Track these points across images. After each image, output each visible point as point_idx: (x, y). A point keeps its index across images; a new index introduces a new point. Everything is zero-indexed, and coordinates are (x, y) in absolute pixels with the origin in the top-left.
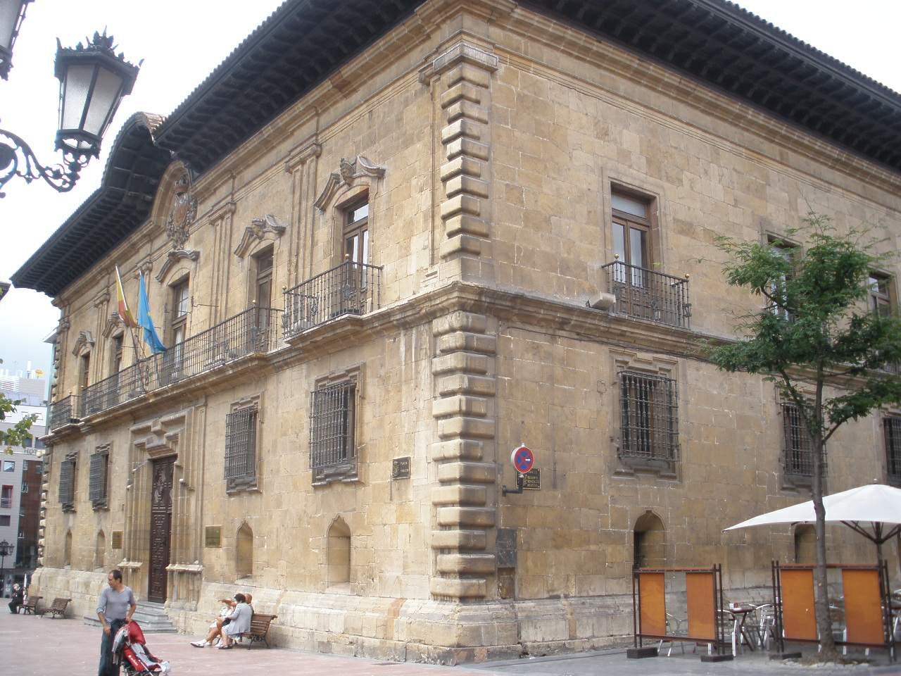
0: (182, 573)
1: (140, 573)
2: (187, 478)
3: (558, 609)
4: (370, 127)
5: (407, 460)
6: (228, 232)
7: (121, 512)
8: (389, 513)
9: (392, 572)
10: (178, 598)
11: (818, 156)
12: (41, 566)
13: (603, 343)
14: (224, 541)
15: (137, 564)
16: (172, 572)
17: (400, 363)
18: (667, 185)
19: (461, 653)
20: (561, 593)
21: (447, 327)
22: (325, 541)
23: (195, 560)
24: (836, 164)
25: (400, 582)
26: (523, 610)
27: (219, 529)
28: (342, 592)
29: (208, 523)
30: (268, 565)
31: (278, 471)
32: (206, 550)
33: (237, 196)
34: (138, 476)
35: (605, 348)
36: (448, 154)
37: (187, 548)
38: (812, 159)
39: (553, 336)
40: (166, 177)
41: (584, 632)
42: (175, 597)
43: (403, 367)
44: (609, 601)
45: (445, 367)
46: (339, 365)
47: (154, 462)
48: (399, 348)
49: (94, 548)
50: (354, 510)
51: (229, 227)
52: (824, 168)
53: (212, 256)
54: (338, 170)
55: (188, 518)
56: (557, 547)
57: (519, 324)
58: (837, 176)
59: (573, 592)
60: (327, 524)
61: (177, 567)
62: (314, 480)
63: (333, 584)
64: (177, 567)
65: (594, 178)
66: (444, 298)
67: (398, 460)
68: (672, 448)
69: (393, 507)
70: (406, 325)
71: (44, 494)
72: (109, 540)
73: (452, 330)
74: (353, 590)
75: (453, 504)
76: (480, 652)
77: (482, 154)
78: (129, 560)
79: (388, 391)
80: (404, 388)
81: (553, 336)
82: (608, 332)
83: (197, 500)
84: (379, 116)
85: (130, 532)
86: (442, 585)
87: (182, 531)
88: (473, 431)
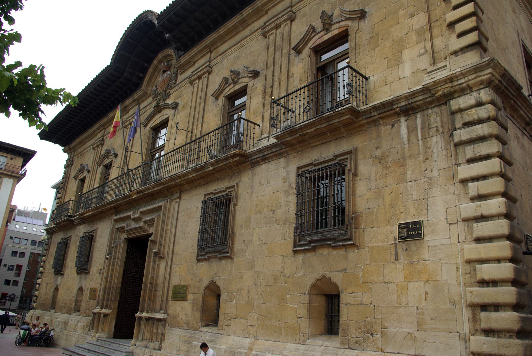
0: (148, 319)
1: (109, 319)
5: (419, 223)
8: (397, 272)
9: (400, 328)
10: (143, 339)
12: (33, 308)
14: (190, 296)
16: (140, 318)
17: (402, 143)
22: (307, 297)
23: (161, 309)
25: (414, 339)
29: (175, 281)
31: (252, 241)
32: (171, 302)
33: (212, 63)
34: (116, 249)
37: (154, 301)
42: (140, 337)
43: (406, 146)
45: (473, 135)
48: (399, 131)
49: (75, 299)
50: (345, 270)
53: (189, 103)
55: (157, 278)
60: (309, 281)
61: (145, 315)
63: (313, 336)
69: (400, 266)
70: (409, 111)
72: (86, 294)
73: (479, 104)
83: (166, 265)
87: (151, 288)
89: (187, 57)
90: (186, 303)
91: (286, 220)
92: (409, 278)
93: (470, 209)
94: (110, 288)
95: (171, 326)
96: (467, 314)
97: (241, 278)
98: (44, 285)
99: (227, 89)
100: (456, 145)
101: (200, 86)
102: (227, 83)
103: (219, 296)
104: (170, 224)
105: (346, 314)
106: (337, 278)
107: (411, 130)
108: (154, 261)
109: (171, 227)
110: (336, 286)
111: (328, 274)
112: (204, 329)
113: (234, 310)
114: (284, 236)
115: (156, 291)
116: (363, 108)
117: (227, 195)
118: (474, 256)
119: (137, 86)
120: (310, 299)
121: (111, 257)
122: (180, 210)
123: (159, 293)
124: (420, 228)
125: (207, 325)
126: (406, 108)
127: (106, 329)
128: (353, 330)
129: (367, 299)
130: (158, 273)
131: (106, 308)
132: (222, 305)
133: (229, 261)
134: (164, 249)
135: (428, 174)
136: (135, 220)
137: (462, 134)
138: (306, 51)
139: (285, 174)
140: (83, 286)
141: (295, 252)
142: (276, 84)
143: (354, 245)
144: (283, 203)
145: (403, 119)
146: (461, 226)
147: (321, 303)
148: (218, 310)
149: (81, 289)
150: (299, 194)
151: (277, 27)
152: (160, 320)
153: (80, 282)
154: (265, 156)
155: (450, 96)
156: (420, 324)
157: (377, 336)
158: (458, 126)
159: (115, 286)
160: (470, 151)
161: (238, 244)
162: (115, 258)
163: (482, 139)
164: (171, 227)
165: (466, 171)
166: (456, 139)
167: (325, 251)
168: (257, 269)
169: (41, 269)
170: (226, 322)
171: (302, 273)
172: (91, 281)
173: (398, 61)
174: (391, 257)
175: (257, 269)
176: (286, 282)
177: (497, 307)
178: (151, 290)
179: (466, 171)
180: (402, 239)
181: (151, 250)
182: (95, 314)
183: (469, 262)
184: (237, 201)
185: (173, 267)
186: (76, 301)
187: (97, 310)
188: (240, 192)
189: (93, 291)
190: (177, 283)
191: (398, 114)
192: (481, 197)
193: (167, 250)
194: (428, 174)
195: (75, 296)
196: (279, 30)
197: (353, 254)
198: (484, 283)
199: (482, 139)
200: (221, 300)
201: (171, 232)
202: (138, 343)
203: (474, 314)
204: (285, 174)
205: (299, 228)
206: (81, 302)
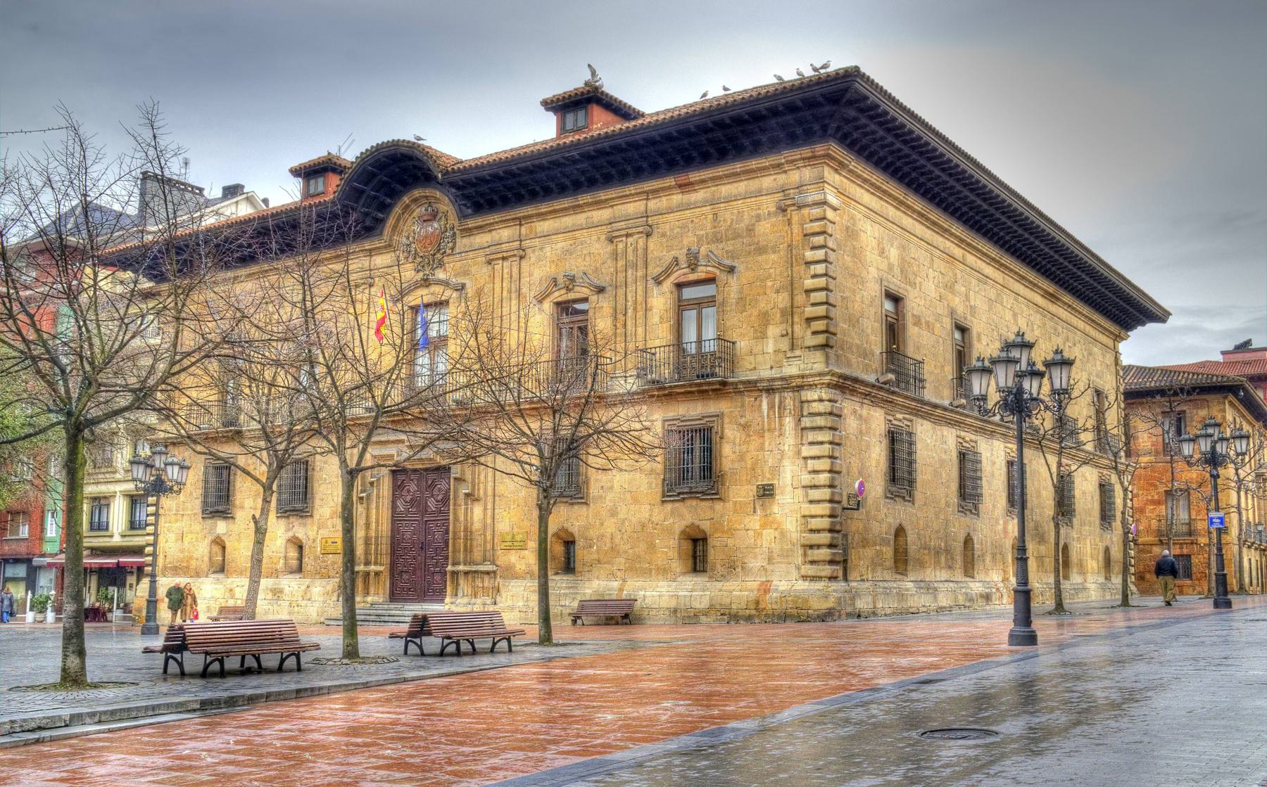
0: (466, 573)
1: (382, 577)
8: (754, 522)
9: (755, 563)
15: (382, 568)
17: (762, 417)
18: (909, 288)
21: (816, 397)
25: (765, 570)
28: (700, 580)
31: (612, 488)
33: (526, 244)
34: (378, 485)
40: (406, 199)
41: (880, 605)
44: (886, 585)
45: (814, 425)
46: (692, 411)
47: (393, 472)
48: (760, 406)
56: (864, 547)
59: (870, 576)
60: (679, 526)
63: (684, 574)
65: (877, 287)
67: (764, 486)
68: (911, 482)
70: (770, 391)
73: (821, 400)
74: (711, 577)
83: (485, 509)
86: (810, 570)
87: (466, 536)
89: (479, 221)
92: (763, 526)
93: (806, 478)
94: (377, 538)
96: (800, 552)
105: (715, 555)
106: (705, 526)
107: (771, 407)
108: (466, 504)
111: (697, 523)
113: (596, 556)
118: (807, 513)
123: (478, 540)
127: (381, 591)
128: (718, 566)
129: (730, 542)
131: (376, 563)
133: (584, 508)
135: (781, 447)
137: (806, 422)
138: (668, 285)
141: (663, 502)
142: (630, 312)
145: (764, 395)
146: (800, 492)
147: (688, 546)
151: (627, 236)
152: (488, 573)
155: (800, 388)
156: (770, 560)
157: (739, 569)
160: (811, 436)
161: (594, 490)
163: (820, 428)
165: (807, 451)
166: (803, 425)
167: (694, 503)
168: (621, 516)
175: (621, 516)
177: (819, 546)
179: (807, 451)
180: (759, 497)
183: (804, 516)
192: (815, 472)
194: (781, 447)
196: (630, 240)
197: (718, 506)
198: (812, 531)
199: (820, 428)
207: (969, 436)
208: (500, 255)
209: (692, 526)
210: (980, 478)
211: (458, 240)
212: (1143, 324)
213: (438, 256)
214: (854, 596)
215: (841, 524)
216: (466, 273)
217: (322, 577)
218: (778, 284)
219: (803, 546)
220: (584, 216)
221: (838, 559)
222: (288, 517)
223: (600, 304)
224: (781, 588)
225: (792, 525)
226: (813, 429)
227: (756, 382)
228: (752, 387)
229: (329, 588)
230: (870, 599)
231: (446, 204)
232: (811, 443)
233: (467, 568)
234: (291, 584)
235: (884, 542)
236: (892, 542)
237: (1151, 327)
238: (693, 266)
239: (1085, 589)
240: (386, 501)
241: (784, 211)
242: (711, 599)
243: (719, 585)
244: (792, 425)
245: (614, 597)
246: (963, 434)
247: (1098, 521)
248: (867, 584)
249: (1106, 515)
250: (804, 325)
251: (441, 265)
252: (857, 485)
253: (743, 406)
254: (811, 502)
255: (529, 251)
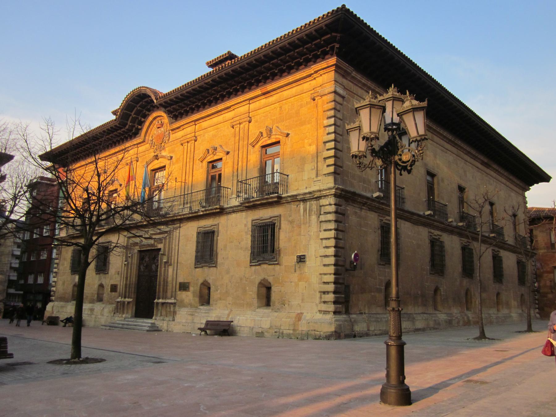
0: (163, 304)
1: (131, 305)
2: (168, 258)
3: (363, 318)
4: (280, 114)
5: (304, 255)
6: (193, 150)
7: (117, 275)
8: (294, 277)
9: (295, 302)
10: (161, 315)
11: (444, 138)
12: (52, 301)
13: (376, 212)
14: (191, 289)
15: (130, 300)
16: (157, 303)
17: (300, 216)
19: (337, 335)
20: (363, 312)
22: (256, 289)
23: (172, 297)
24: (450, 142)
25: (300, 306)
26: (353, 318)
27: (189, 283)
28: (266, 311)
29: (181, 279)
30: (220, 299)
31: (228, 258)
32: (179, 293)
34: (132, 258)
35: (376, 214)
36: (327, 132)
37: (166, 292)
38: (442, 139)
39: (361, 209)
41: (372, 328)
42: (159, 315)
43: (302, 218)
44: (378, 316)
45: (327, 219)
46: (265, 214)
49: (96, 292)
50: (274, 275)
51: (193, 147)
52: (445, 143)
53: (181, 159)
54: (263, 130)
55: (167, 278)
56: (362, 293)
57: (351, 204)
58: (448, 146)
59: (367, 312)
60: (257, 282)
61: (160, 301)
62: (251, 262)
63: (259, 307)
64: (160, 301)
66: (328, 191)
67: (300, 256)
69: (296, 275)
70: (304, 200)
71: (55, 265)
72: (108, 289)
74: (272, 310)
75: (330, 274)
76: (342, 335)
77: (341, 133)
78: (125, 298)
79: (293, 227)
80: (302, 226)
81: (361, 209)
82: (378, 208)
83: (173, 270)
84: (285, 110)
85: (126, 285)
86: (324, 307)
87: (164, 283)
88: (339, 246)
90: (189, 293)
91: (246, 248)
92: (300, 280)
94: (130, 284)
95: (180, 307)
96: (318, 295)
97: (222, 278)
98: (60, 283)
99: (209, 157)
100: (320, 222)
101: (189, 148)
102: (208, 153)
103: (209, 289)
104: (174, 244)
105: (274, 296)
106: (270, 279)
107: (305, 210)
108: (165, 267)
109: (175, 246)
110: (270, 283)
111: (266, 277)
112: (201, 307)
113: (219, 296)
114: (246, 256)
115: (167, 286)
116: (283, 196)
117: (271, 222)
118: (322, 272)
119: (136, 133)
120: (258, 290)
121: (128, 263)
122: (181, 235)
123: (170, 287)
124: (304, 258)
125: (202, 305)
126: (303, 199)
127: (130, 311)
128: (276, 303)
130: (168, 275)
131: (128, 298)
132: (211, 294)
134: (171, 260)
136: (147, 238)
137: (323, 218)
139: (245, 222)
140: (103, 283)
143: (277, 264)
144: (244, 239)
145: (302, 203)
146: (319, 259)
147: (264, 290)
148: (209, 297)
149: (101, 286)
150: (253, 236)
152: (172, 303)
153: (100, 279)
154: (234, 210)
156: (303, 300)
158: (322, 213)
159: (134, 283)
161: (220, 260)
162: (131, 264)
164: (175, 246)
166: (320, 220)
169: (55, 270)
170: (215, 303)
171: (254, 277)
172: (110, 279)
173: (303, 170)
174: (293, 270)
176: (246, 281)
178: (164, 286)
181: (162, 260)
182: (118, 302)
183: (321, 274)
184: (218, 234)
185: (178, 271)
186: (98, 294)
187: (119, 299)
188: (220, 229)
189: (114, 288)
190: (182, 281)
191: (299, 201)
193: (174, 259)
195: (97, 290)
197: (277, 267)
200: (211, 291)
201: (175, 249)
202: (158, 318)
203: (321, 296)
204: (245, 222)
205: (253, 253)
206: (103, 294)
207: (437, 232)
208: (186, 141)
209: (264, 279)
210: (444, 256)
211: (171, 136)
212: (537, 183)
213: (163, 144)
214: (352, 323)
215: (344, 279)
216: (173, 151)
217: (110, 304)
218: (310, 141)
219: (320, 292)
220: (222, 116)
221: (340, 300)
222: (99, 274)
223: (228, 161)
224: (307, 318)
225: (315, 280)
226: (326, 221)
227: (296, 195)
228: (295, 199)
229: (111, 309)
230: (365, 325)
231: (162, 115)
232: (325, 230)
233: (164, 301)
234: (98, 307)
235: (379, 291)
236: (383, 291)
237: (542, 184)
238: (270, 135)
239: (511, 317)
240: (135, 266)
241: (314, 100)
242: (271, 323)
243: (276, 314)
244: (316, 220)
245: (225, 320)
246: (432, 231)
247: (516, 281)
248: (364, 316)
249: (522, 280)
250: (323, 162)
251: (164, 149)
252: (353, 256)
253: (291, 210)
254: (324, 265)
255: (198, 138)
